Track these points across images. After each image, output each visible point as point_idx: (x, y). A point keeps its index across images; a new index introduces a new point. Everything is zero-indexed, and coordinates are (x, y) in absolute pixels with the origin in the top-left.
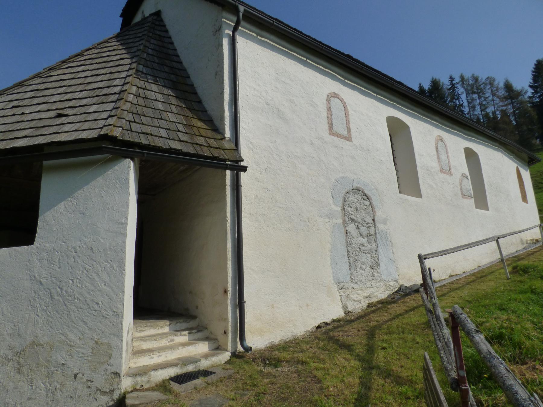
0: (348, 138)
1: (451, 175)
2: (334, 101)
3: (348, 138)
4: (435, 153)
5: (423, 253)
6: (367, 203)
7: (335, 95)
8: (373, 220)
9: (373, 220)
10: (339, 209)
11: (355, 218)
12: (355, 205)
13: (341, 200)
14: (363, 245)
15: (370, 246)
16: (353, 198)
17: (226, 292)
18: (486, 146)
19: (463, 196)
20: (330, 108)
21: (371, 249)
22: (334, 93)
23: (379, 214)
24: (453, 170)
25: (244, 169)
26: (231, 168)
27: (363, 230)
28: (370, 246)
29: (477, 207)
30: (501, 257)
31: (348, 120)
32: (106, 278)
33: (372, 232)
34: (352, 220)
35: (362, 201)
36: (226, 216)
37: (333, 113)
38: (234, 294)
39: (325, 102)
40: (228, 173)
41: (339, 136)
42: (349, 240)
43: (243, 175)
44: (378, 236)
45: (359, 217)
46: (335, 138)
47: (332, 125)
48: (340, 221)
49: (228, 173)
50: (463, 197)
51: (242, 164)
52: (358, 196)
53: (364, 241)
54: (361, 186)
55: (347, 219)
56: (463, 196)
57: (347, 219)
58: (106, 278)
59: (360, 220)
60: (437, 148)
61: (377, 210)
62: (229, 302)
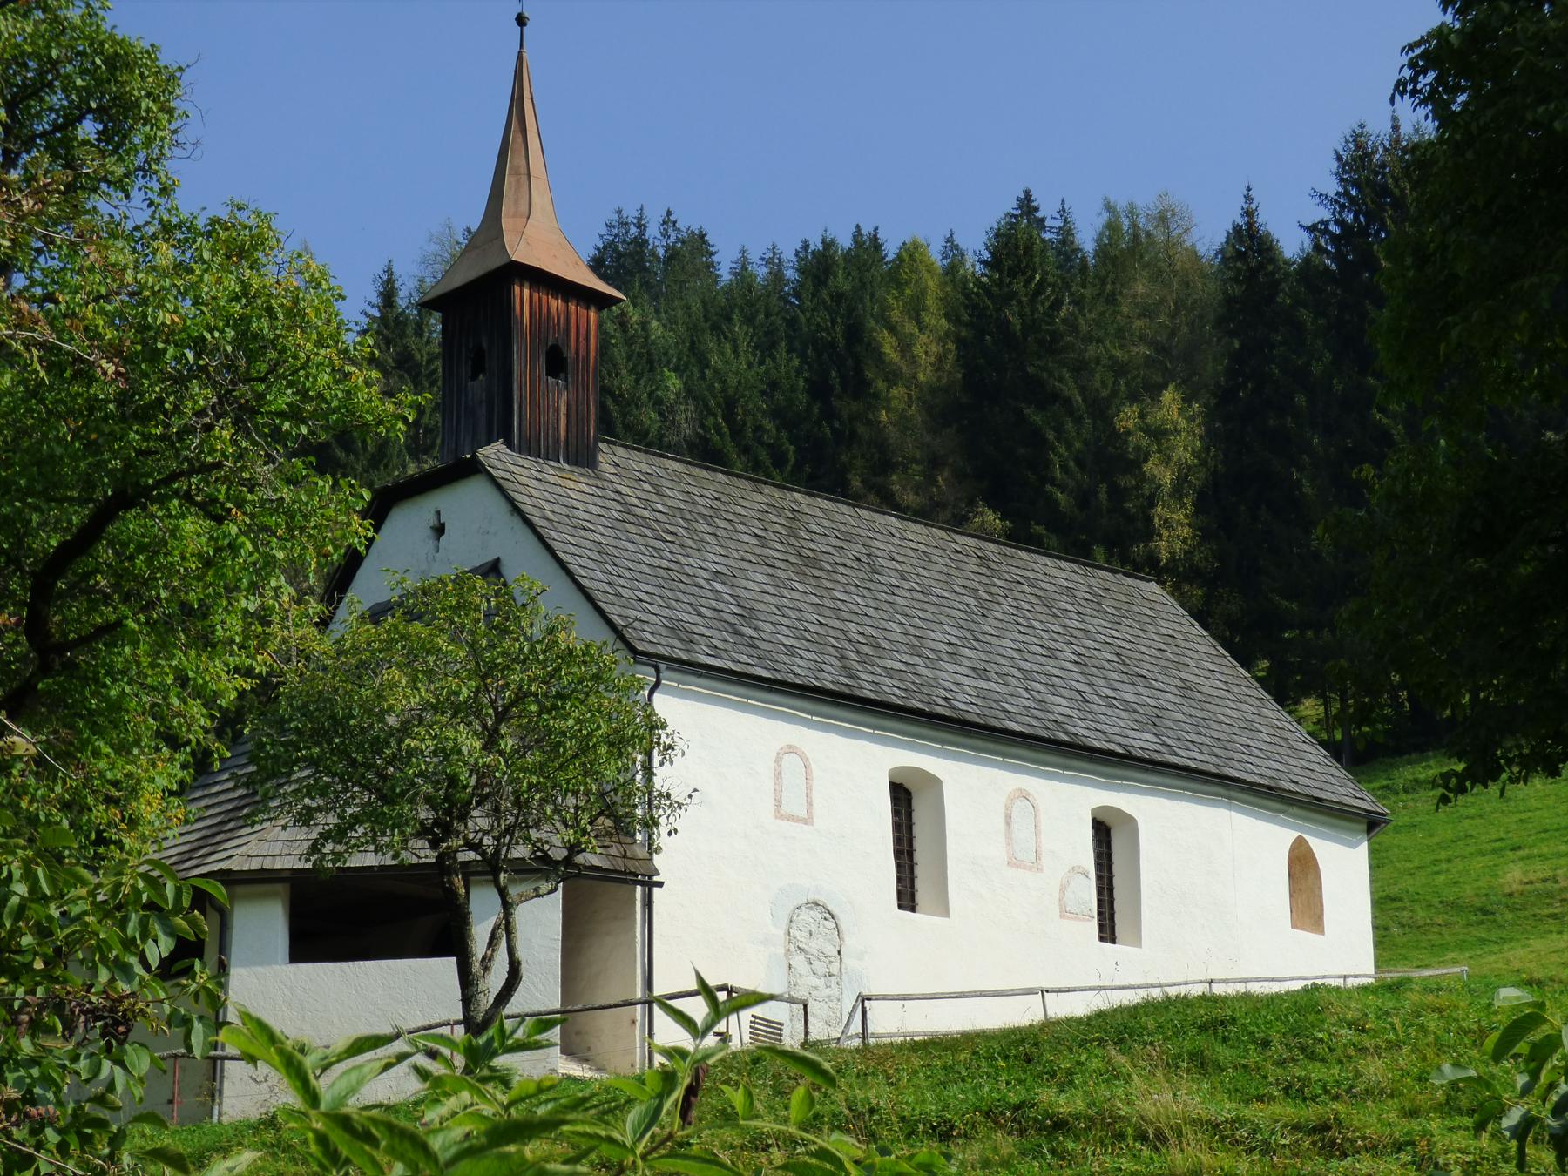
0: (808, 821)
1: (1040, 870)
2: (791, 761)
3: (808, 821)
4: (1002, 825)
5: (866, 992)
6: (831, 924)
7: (792, 749)
8: (839, 952)
9: (839, 952)
10: (781, 933)
11: (807, 948)
12: (809, 928)
13: (786, 920)
14: (816, 988)
15: (827, 992)
16: (806, 916)
17: (634, 1022)
18: (1169, 796)
19: (1064, 913)
20: (780, 773)
21: (829, 997)
22: (790, 746)
23: (850, 943)
24: (1045, 861)
25: (660, 884)
26: (642, 883)
27: (819, 967)
28: (827, 992)
29: (1294, 926)
30: (279, 887)
31: (809, 789)
32: (542, 989)
33: (835, 970)
34: (802, 950)
35: (823, 921)
36: (635, 937)
37: (784, 782)
38: (643, 1025)
39: (773, 764)
40: (639, 888)
41: (791, 818)
42: (792, 979)
43: (656, 890)
44: (844, 977)
45: (812, 946)
46: (785, 824)
47: (780, 801)
48: (782, 951)
49: (639, 888)
50: (1062, 916)
51: (656, 879)
52: (816, 914)
53: (820, 983)
54: (818, 898)
55: (792, 948)
56: (1064, 913)
57: (792, 948)
58: (542, 989)
59: (815, 952)
60: (1008, 818)
61: (846, 936)
62: (637, 1033)
